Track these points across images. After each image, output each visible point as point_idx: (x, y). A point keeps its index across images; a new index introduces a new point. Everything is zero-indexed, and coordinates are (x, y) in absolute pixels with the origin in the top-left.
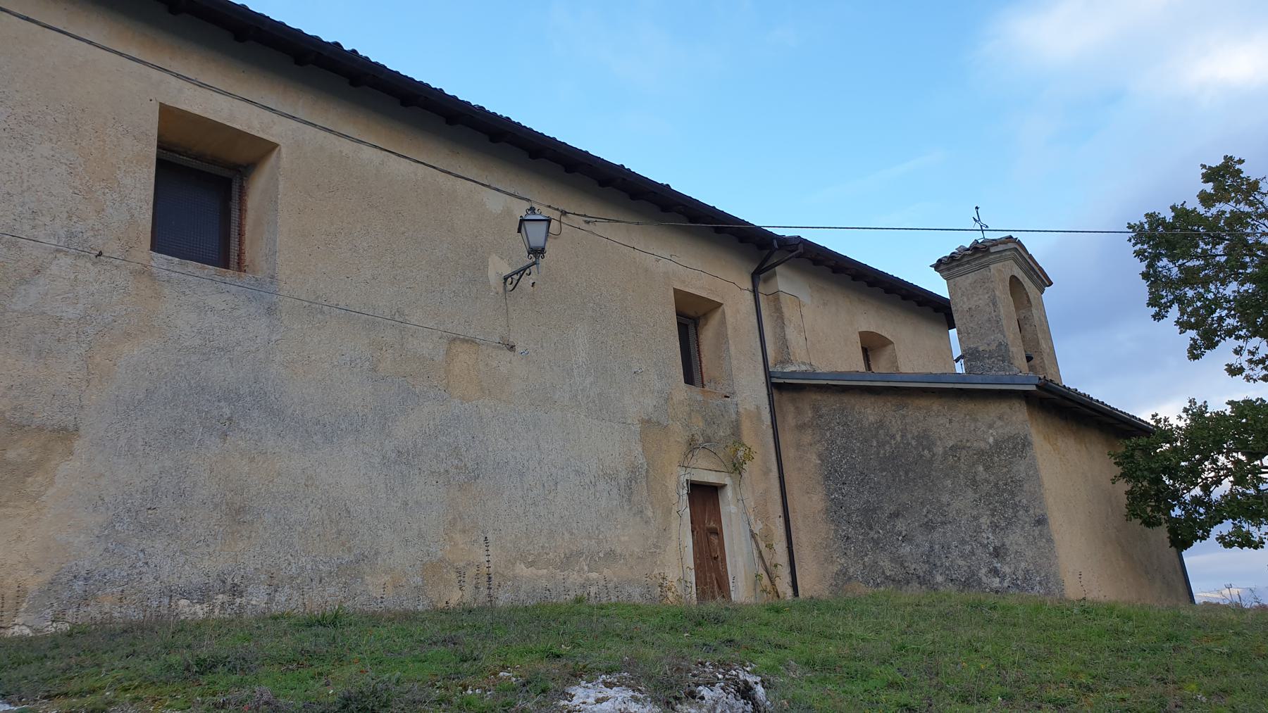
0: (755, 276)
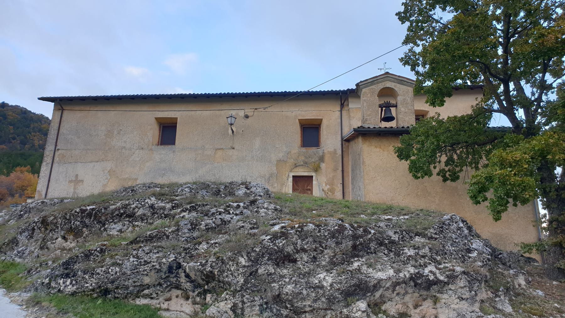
0: (342, 106)
